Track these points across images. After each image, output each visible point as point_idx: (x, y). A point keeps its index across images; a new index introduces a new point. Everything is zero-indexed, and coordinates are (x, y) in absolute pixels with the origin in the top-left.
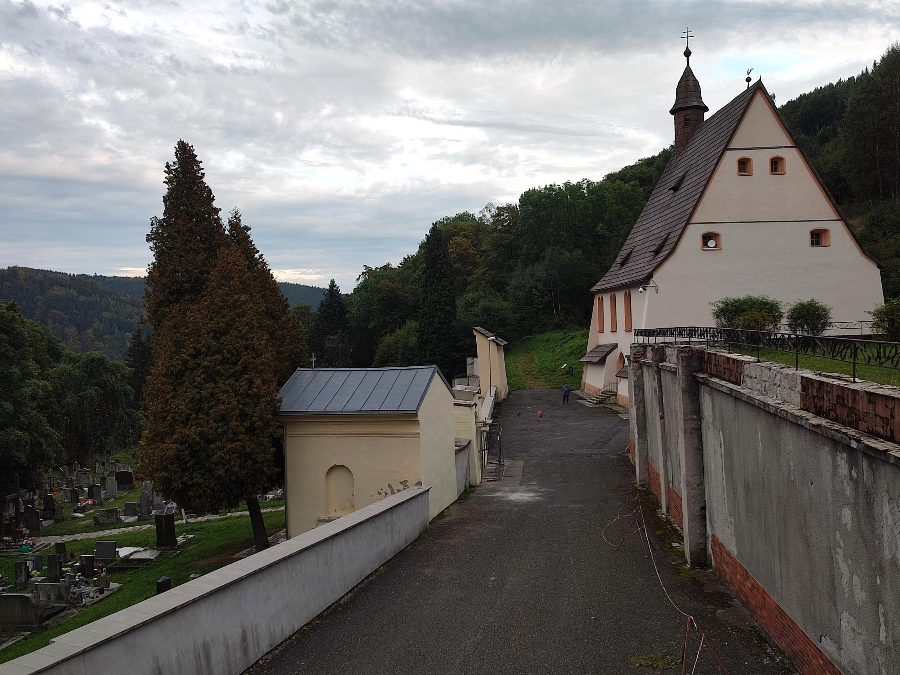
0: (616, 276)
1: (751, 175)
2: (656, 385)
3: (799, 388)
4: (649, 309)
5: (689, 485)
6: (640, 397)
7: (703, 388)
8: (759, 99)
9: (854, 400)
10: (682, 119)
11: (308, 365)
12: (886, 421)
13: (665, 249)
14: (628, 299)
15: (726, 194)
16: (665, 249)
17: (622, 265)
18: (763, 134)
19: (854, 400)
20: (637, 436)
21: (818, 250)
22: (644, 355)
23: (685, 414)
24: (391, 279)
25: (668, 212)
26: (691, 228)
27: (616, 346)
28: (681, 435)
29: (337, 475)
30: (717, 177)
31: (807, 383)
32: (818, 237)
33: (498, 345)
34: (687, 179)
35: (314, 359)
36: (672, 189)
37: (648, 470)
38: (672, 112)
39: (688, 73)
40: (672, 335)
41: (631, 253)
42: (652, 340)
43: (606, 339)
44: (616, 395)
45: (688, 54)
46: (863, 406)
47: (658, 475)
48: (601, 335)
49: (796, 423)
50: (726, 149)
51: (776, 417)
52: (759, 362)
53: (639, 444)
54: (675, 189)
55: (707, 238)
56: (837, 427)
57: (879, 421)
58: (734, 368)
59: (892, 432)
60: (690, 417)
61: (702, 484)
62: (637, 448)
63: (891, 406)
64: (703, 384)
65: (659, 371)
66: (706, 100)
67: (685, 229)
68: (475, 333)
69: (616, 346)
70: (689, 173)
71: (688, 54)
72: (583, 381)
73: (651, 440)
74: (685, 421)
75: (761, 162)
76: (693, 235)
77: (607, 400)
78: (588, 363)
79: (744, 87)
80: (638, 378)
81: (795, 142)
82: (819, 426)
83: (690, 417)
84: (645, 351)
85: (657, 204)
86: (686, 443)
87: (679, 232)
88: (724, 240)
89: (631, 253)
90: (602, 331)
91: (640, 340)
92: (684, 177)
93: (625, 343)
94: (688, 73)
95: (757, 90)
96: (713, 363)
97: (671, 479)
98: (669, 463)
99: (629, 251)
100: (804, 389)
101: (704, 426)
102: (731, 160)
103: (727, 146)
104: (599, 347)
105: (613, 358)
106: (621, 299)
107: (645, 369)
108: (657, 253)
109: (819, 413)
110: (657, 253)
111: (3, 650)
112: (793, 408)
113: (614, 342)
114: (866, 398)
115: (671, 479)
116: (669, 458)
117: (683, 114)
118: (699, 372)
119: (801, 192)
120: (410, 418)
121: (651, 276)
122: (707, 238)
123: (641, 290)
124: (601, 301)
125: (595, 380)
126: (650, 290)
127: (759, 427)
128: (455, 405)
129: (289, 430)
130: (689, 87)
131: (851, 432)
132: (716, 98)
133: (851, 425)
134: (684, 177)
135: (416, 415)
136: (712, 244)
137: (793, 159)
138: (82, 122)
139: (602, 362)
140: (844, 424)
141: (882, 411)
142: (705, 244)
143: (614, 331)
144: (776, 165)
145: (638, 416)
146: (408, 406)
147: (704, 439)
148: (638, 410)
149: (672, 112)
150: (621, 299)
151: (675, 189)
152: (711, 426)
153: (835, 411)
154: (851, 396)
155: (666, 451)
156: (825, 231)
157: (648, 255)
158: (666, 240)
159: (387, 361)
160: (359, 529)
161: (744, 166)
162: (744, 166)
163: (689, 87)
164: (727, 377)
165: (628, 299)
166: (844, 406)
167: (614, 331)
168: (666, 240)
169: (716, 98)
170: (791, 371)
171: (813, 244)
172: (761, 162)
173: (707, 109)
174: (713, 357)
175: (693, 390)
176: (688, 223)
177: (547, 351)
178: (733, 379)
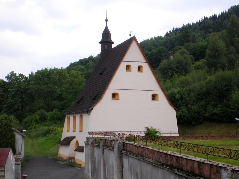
2: (103, 155)
15: (120, 79)
18: (134, 55)
21: (154, 102)
27: (74, 137)
32: (154, 97)
38: (100, 43)
43: (70, 134)
45: (107, 20)
54: (101, 74)
66: (113, 39)
69: (74, 137)
70: (107, 68)
71: (107, 20)
75: (134, 67)
76: (108, 94)
79: (128, 38)
88: (120, 96)
90: (68, 131)
95: (133, 39)
102: (123, 66)
105: (73, 142)
111: (93, 175)
119: (148, 80)
124: (69, 118)
130: (106, 34)
132: (117, 40)
137: (146, 67)
138: (125, 159)
143: (74, 131)
144: (140, 68)
148: (92, 165)
149: (100, 43)
161: (128, 67)
162: (128, 67)
163: (106, 34)
167: (74, 131)
169: (117, 40)
171: (152, 99)
172: (134, 67)
173: (113, 43)
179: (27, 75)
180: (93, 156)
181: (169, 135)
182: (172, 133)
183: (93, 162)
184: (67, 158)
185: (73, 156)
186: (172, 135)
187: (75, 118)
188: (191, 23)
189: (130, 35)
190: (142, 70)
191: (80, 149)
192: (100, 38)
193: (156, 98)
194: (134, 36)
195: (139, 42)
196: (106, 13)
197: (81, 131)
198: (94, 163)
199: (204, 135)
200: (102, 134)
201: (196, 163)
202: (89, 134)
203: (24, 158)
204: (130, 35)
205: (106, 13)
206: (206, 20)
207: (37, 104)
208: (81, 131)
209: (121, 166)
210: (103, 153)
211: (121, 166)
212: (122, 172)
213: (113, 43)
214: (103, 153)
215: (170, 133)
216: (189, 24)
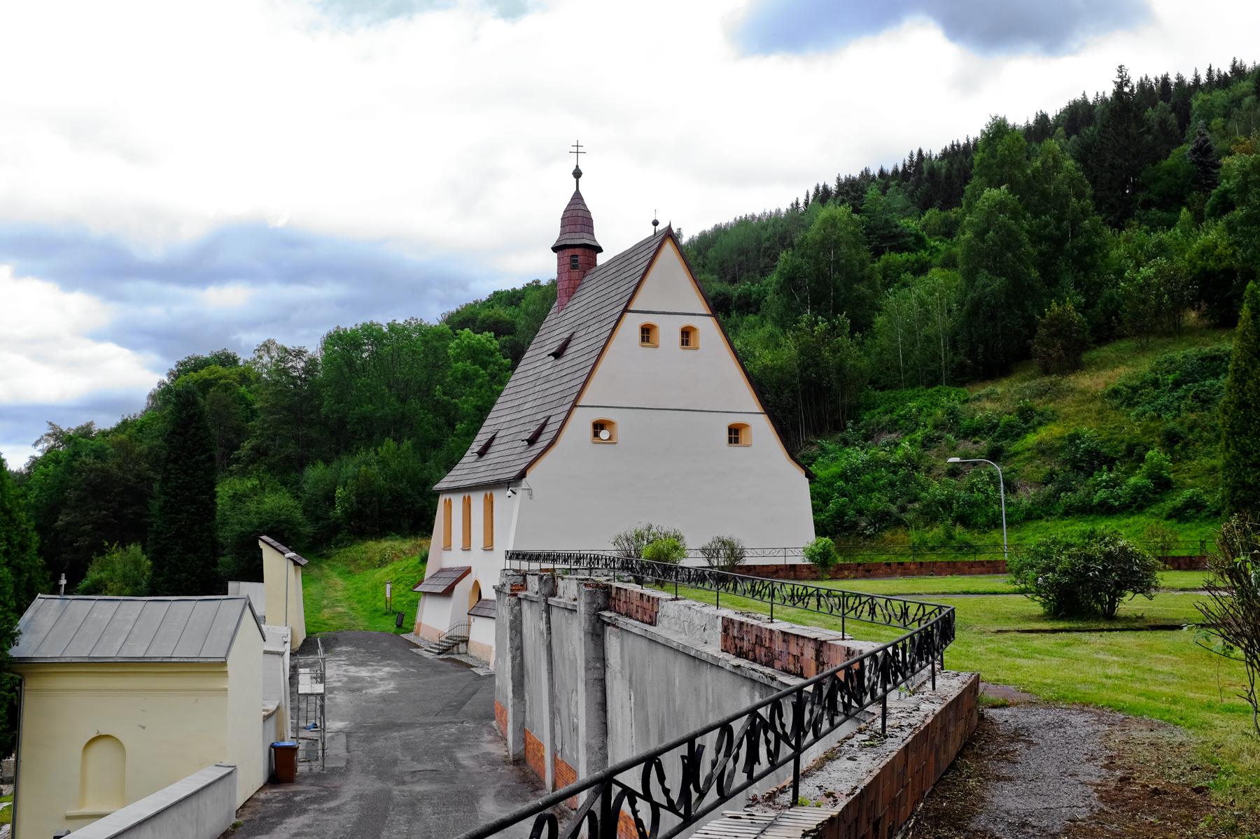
0: (468, 469)
1: (657, 347)
2: (543, 626)
3: (720, 629)
4: (515, 522)
5: (589, 747)
6: (517, 642)
7: (609, 629)
8: (668, 248)
9: (771, 640)
10: (568, 260)
11: (55, 590)
12: (796, 658)
13: (542, 438)
14: (489, 504)
16: (539, 439)
17: (481, 454)
18: (675, 294)
19: (771, 640)
20: (510, 695)
21: (735, 450)
22: (524, 586)
23: (587, 662)
24: (99, 454)
25: (547, 386)
26: (577, 411)
27: (468, 571)
28: (581, 687)
29: (98, 747)
31: (727, 624)
32: (735, 433)
33: (296, 563)
34: (572, 343)
35: (63, 582)
36: (553, 354)
37: (525, 740)
38: (555, 249)
39: (577, 197)
40: (565, 561)
41: (493, 438)
42: (535, 566)
43: (455, 559)
45: (577, 174)
46: (778, 646)
47: (540, 745)
48: (445, 552)
49: (715, 665)
50: (626, 310)
51: (697, 660)
52: (677, 599)
53: (513, 706)
54: (558, 355)
55: (599, 426)
56: (756, 666)
57: (791, 658)
58: (647, 605)
59: (802, 668)
60: (592, 664)
62: (510, 711)
63: (801, 643)
64: (609, 624)
65: (548, 608)
67: (570, 412)
68: (261, 544)
69: (468, 571)
70: (576, 335)
71: (577, 174)
72: (418, 621)
74: (587, 669)
75: (668, 331)
76: (582, 421)
77: (453, 646)
78: (425, 593)
79: (649, 231)
80: (515, 617)
82: (739, 666)
83: (592, 664)
84: (525, 580)
85: (531, 373)
86: (587, 697)
88: (621, 431)
89: (493, 438)
90: (448, 547)
91: (516, 564)
92: (569, 340)
93: (489, 572)
94: (577, 197)
96: (623, 599)
97: (559, 747)
98: (558, 728)
99: (490, 436)
100: (725, 629)
101: (608, 675)
102: (632, 324)
103: (630, 301)
104: (442, 570)
107: (525, 605)
108: (532, 441)
109: (740, 654)
110: (532, 441)
112: (713, 648)
113: (466, 564)
114: (781, 637)
115: (559, 747)
116: (557, 721)
117: (569, 252)
118: (605, 609)
119: (714, 376)
120: (218, 666)
121: (522, 475)
122: (599, 426)
123: (509, 493)
124: (449, 504)
125: (435, 619)
127: (679, 668)
128: (266, 652)
129: (30, 685)
130: (577, 216)
131: (768, 670)
132: (616, 236)
133: (767, 665)
134: (569, 340)
135: (224, 664)
136: (604, 434)
137: (708, 329)
139: (448, 592)
140: (761, 663)
141: (794, 650)
142: (596, 435)
143: (467, 547)
145: (513, 667)
146: (212, 651)
147: (608, 691)
148: (513, 659)
149: (555, 249)
151: (558, 355)
152: (619, 675)
153: (754, 651)
154: (768, 636)
155: (554, 712)
156: (745, 426)
157: (516, 444)
158: (544, 426)
159: (96, 589)
160: (165, 816)
161: (647, 332)
162: (647, 332)
163: (577, 216)
164: (639, 616)
165: (489, 504)
166: (762, 645)
167: (467, 547)
168: (544, 426)
170: (711, 610)
172: (668, 331)
173: (599, 250)
174: (623, 593)
175: (597, 631)
176: (575, 405)
177: (372, 573)
178: (646, 618)
179: (313, 347)
180: (516, 627)
181: (780, 561)
182: (789, 553)
183: (518, 650)
184: (443, 639)
185: (460, 632)
186: (790, 561)
189: (655, 223)
191: (479, 607)
192: (553, 231)
193: (743, 436)
194: (262, 581)
195: (684, 240)
196: (575, 149)
197: (489, 547)
198: (522, 654)
200: (554, 560)
201: (811, 644)
202: (511, 558)
203: (329, 360)
204: (655, 223)
205: (575, 149)
208: (489, 547)
209: (599, 659)
210: (548, 621)
211: (599, 659)
213: (599, 250)
214: (548, 621)
215: (782, 553)
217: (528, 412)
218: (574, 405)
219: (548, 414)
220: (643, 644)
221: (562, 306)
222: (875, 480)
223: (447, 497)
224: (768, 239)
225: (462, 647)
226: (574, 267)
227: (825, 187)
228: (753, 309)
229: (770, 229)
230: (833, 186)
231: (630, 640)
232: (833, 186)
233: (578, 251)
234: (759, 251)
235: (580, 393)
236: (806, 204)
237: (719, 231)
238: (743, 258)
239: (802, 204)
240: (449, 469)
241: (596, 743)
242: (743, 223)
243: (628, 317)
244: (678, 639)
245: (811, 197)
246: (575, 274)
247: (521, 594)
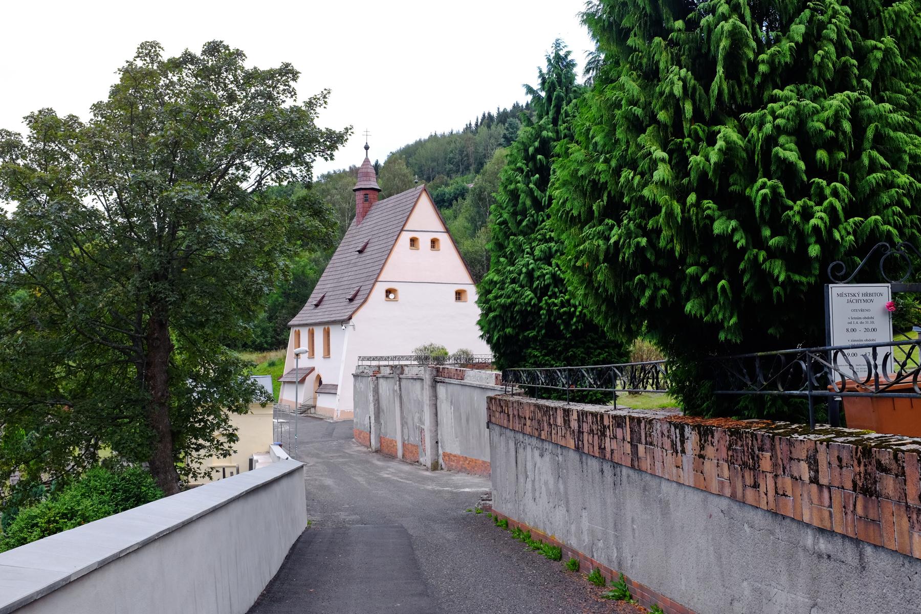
0: (306, 314)
14: (327, 334)
16: (356, 299)
21: (460, 304)
26: (378, 284)
27: (313, 369)
30: (396, 249)
32: (459, 295)
43: (304, 362)
44: (314, 407)
45: (367, 148)
50: (402, 230)
55: (388, 292)
61: (436, 431)
67: (374, 284)
69: (313, 369)
71: (367, 148)
73: (386, 423)
75: (424, 241)
76: (379, 290)
81: (446, 229)
87: (370, 286)
88: (400, 294)
98: (406, 431)
102: (405, 237)
105: (311, 379)
106: (319, 333)
108: (351, 300)
121: (350, 318)
122: (388, 292)
124: (298, 334)
126: (350, 328)
136: (392, 296)
137: (445, 240)
139: (302, 381)
142: (387, 296)
144: (434, 243)
150: (319, 333)
156: (464, 291)
162: (413, 241)
165: (327, 334)
172: (424, 241)
185: (311, 403)
187: (312, 335)
188: (439, 133)
190: (439, 247)
193: (463, 297)
199: (393, 470)
206: (484, 129)
207: (37, 337)
208: (327, 353)
209: (435, 396)
212: (436, 405)
216: (239, 54)
217: (346, 283)
218: (376, 281)
219: (360, 284)
220: (459, 387)
221: (359, 222)
222: (232, 82)
223: (297, 329)
224: (452, 152)
225: (312, 410)
226: (366, 200)
227: (489, 114)
228: (446, 204)
229: (453, 145)
230: (494, 113)
231: (450, 388)
232: (494, 113)
233: (367, 192)
234: (446, 158)
235: (379, 274)
236: (476, 125)
237: (420, 144)
238: (435, 164)
239: (473, 125)
240: (294, 316)
241: (433, 429)
242: (433, 138)
243: (404, 233)
244: (476, 383)
245: (480, 121)
246: (367, 204)
247: (379, 375)
